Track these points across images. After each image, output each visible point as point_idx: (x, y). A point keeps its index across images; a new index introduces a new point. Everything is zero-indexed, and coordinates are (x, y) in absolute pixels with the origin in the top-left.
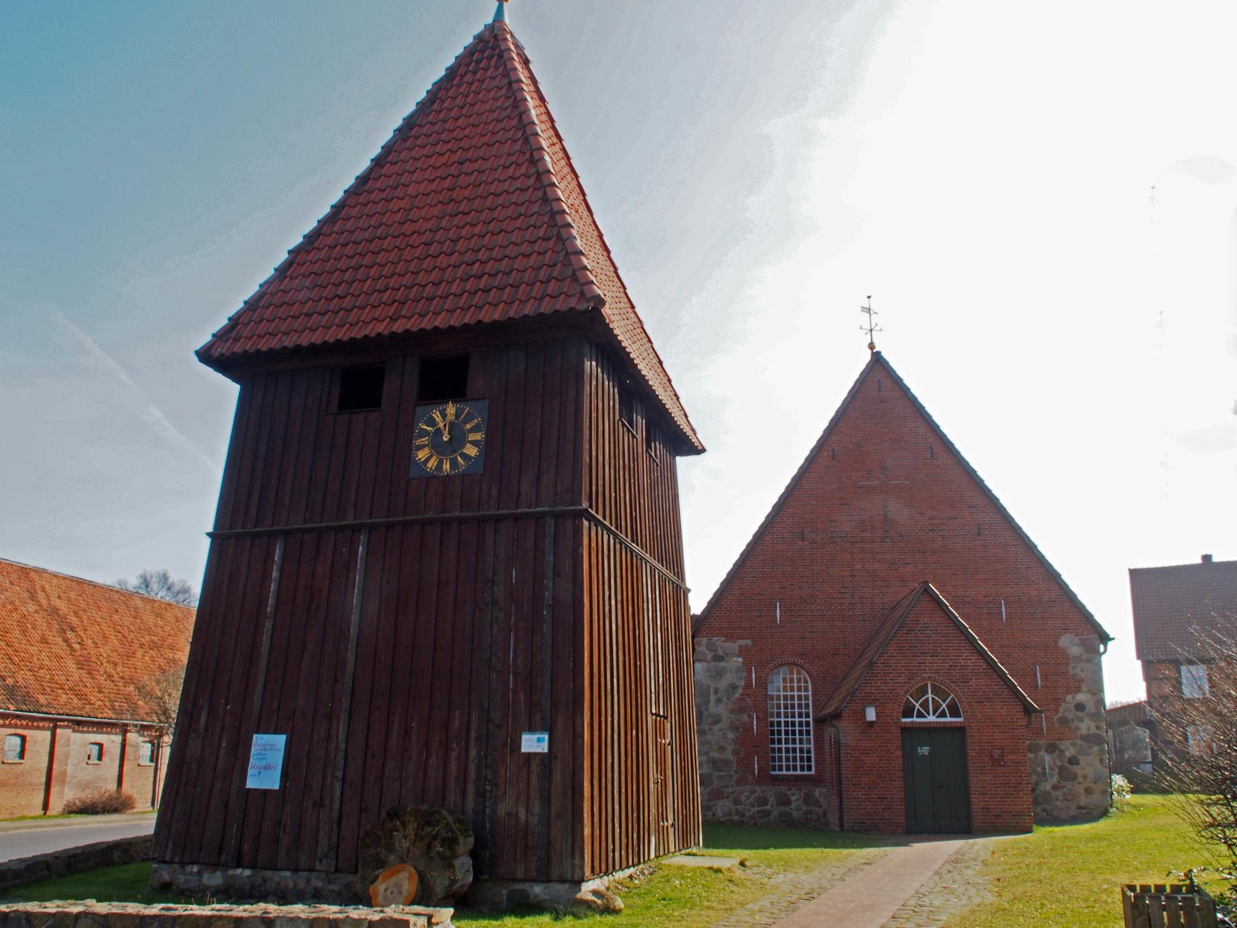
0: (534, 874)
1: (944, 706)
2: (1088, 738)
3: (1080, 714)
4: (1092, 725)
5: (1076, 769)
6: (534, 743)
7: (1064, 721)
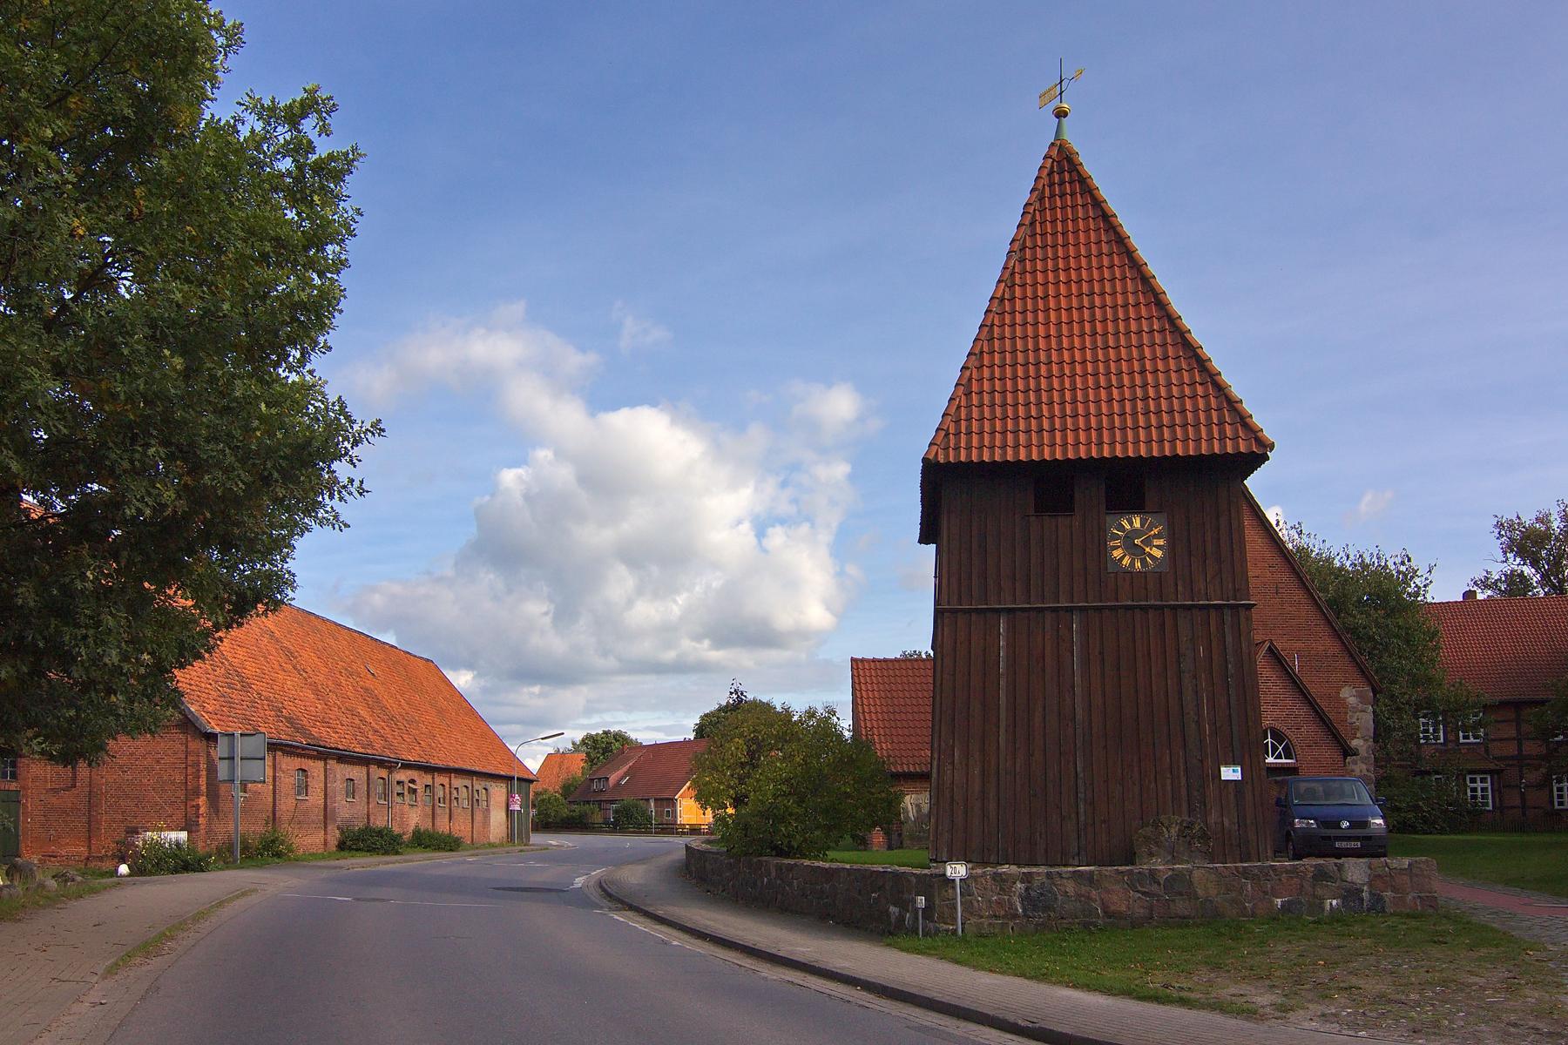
6: (1230, 773)
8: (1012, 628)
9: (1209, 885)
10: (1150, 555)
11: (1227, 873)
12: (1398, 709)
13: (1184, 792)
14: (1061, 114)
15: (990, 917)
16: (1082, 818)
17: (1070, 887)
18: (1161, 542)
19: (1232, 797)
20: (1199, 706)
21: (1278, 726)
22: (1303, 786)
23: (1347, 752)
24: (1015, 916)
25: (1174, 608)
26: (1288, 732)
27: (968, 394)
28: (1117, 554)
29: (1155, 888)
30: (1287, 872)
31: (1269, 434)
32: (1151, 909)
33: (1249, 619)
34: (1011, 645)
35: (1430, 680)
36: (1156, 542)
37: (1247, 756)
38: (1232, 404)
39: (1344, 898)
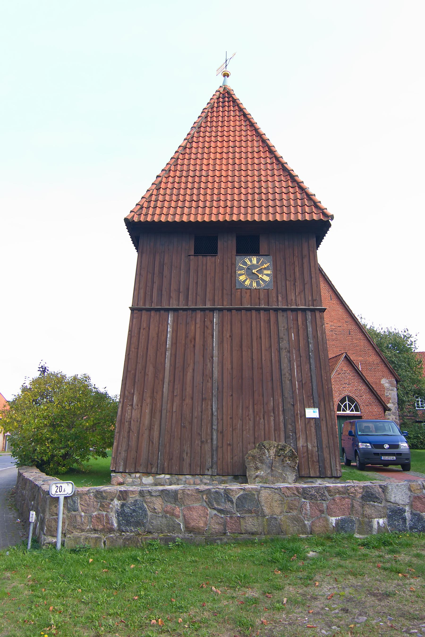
0: (318, 474)
1: (353, 406)
4: (394, 417)
6: (312, 413)
8: (176, 321)
9: (275, 504)
10: (262, 279)
11: (288, 493)
12: (407, 393)
13: (282, 425)
14: (226, 75)
15: (90, 531)
16: (215, 442)
17: (158, 504)
18: (269, 272)
19: (313, 430)
20: (291, 370)
21: (351, 395)
22: (365, 424)
23: (386, 409)
24: (111, 530)
25: (276, 310)
26: (356, 398)
27: (158, 189)
28: (242, 278)
29: (228, 506)
30: (339, 492)
31: (330, 211)
32: (225, 525)
33: (322, 318)
34: (175, 331)
35: (419, 381)
36: (266, 272)
37: (322, 399)
38: (309, 197)
39: (390, 517)
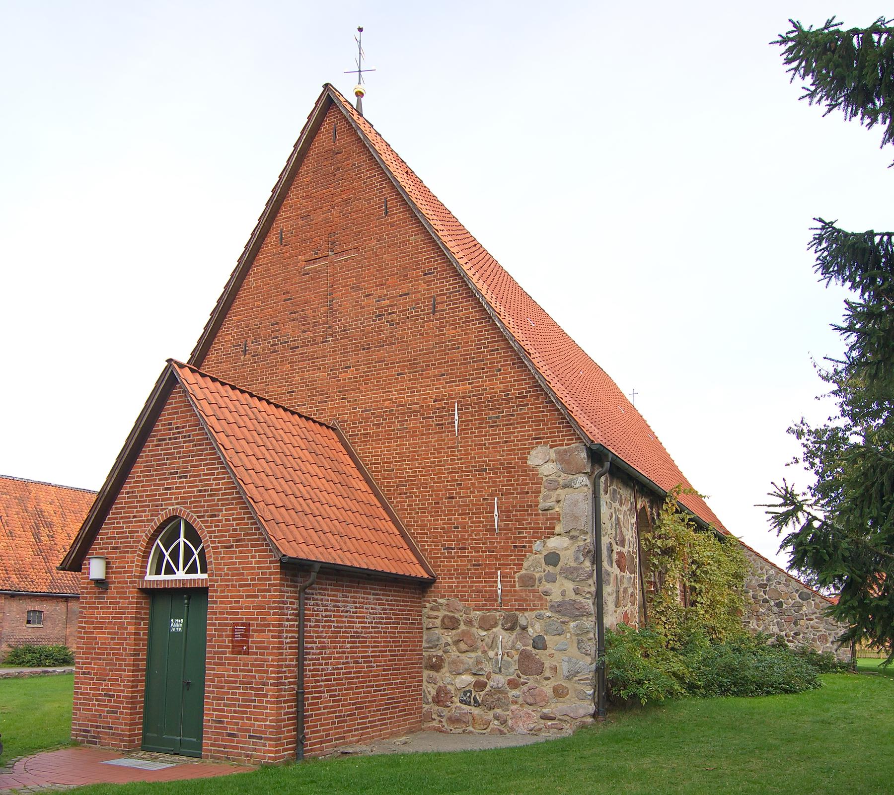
2: (558, 608)
3: (550, 569)
4: (569, 586)
5: (540, 654)
7: (528, 581)
